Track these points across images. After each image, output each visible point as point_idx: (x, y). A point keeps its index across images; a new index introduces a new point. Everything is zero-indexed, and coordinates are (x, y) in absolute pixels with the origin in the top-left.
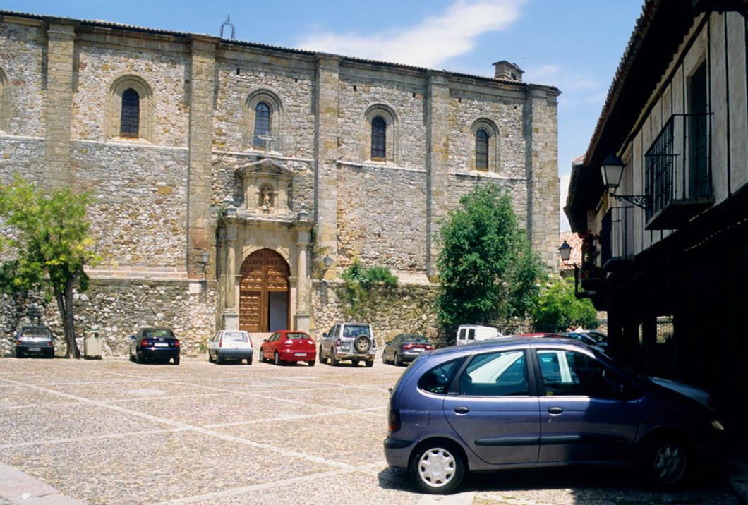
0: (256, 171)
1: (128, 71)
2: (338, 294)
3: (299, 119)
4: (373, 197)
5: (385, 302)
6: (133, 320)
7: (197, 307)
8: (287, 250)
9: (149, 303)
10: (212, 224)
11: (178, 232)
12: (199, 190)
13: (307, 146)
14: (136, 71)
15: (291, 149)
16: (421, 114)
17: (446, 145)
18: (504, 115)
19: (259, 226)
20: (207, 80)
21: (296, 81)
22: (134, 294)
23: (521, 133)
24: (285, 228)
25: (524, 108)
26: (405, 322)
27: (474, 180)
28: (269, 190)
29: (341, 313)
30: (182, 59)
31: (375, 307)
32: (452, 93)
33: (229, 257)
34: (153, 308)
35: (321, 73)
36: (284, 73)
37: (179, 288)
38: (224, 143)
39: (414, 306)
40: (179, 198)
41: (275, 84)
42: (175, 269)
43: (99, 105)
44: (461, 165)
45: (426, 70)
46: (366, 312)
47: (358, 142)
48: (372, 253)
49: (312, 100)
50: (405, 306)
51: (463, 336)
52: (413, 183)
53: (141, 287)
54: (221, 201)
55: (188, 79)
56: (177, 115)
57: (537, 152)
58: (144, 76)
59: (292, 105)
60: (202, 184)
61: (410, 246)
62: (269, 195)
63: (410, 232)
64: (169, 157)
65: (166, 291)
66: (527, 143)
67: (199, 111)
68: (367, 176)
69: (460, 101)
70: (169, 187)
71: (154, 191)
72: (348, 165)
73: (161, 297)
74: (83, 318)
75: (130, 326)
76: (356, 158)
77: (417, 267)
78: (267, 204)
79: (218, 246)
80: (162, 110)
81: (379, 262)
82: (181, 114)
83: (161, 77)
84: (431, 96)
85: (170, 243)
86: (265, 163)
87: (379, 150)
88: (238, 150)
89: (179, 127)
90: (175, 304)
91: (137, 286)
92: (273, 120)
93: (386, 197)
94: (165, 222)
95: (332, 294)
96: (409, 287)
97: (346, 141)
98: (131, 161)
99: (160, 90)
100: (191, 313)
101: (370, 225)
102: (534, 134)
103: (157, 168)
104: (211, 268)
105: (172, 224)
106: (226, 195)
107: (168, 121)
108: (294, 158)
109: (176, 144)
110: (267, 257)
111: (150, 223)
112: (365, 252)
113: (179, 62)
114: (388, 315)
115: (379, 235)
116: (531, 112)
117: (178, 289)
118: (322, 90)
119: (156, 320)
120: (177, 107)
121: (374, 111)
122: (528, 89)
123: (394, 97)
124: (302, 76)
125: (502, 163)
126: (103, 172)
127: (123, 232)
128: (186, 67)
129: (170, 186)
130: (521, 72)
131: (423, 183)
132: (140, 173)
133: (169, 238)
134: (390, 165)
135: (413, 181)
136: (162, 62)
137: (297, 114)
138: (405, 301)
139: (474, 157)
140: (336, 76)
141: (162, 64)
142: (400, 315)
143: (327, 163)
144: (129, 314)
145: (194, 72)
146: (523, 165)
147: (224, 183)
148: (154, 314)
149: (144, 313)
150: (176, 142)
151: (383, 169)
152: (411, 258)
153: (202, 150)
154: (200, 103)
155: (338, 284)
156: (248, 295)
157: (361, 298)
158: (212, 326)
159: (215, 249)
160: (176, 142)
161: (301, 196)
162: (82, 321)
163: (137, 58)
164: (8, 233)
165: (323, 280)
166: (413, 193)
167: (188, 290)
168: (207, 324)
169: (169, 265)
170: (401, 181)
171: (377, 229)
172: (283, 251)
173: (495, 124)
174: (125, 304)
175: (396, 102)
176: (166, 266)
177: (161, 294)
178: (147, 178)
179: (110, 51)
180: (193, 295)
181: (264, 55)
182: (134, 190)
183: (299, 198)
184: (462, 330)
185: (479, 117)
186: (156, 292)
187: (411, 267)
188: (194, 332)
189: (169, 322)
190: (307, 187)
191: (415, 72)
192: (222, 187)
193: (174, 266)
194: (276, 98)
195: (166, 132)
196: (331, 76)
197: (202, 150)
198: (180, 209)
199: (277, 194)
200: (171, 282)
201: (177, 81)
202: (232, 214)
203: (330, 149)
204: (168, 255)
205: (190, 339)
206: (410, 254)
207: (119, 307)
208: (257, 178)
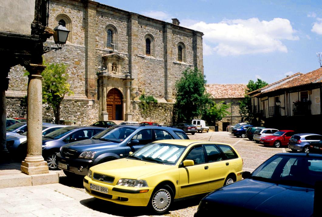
0: (111, 57)
1: (62, 12)
2: (139, 106)
3: (123, 37)
4: (148, 69)
5: (154, 109)
6: (69, 116)
7: (92, 111)
8: (122, 89)
9: (74, 109)
10: (96, 78)
11: (82, 80)
12: (91, 64)
13: (126, 48)
14: (65, 12)
15: (120, 49)
16: (162, 39)
17: (171, 51)
18: (187, 41)
19: (113, 79)
20: (93, 19)
21: (122, 22)
22: (69, 105)
23: (192, 48)
24: (122, 80)
25: (193, 39)
26: (160, 116)
27: (179, 65)
28: (115, 65)
29: (140, 113)
30: (82, 9)
31: (151, 111)
32: (174, 33)
33: (104, 91)
34: (76, 111)
35: (132, 20)
36: (118, 19)
37: (86, 103)
38: (97, 45)
39: (163, 111)
40: (83, 66)
41: (115, 23)
42: (82, 95)
43: (51, 25)
44: (174, 59)
45: (164, 22)
46: (148, 113)
47: (142, 48)
48: (148, 91)
49: (127, 31)
50: (160, 111)
51: (195, 123)
53: (71, 102)
54: (97, 68)
55: (84, 18)
56: (81, 32)
57: (198, 56)
58: (68, 15)
59: (121, 32)
60: (92, 61)
61: (159, 88)
62: (115, 67)
63: (159, 83)
64: (78, 49)
65: (81, 104)
66: (194, 52)
67: (91, 32)
68: (146, 61)
69: (174, 35)
70: (79, 62)
71: (73, 63)
72: (140, 56)
73: (79, 106)
74: (50, 114)
75: (67, 118)
76: (142, 54)
77: (162, 96)
78: (115, 71)
79: (98, 86)
80: (75, 30)
81: (150, 94)
82: (82, 32)
83: (75, 16)
84: (167, 32)
85: (80, 84)
86: (115, 54)
87: (148, 52)
88: (103, 49)
89: (82, 37)
90: (84, 109)
91: (70, 102)
92: (114, 37)
93: (152, 70)
94: (78, 76)
95: (137, 106)
96: (161, 104)
98: (65, 50)
99: (74, 21)
100: (90, 113)
101: (147, 80)
102: (197, 49)
103: (74, 54)
104: (96, 96)
105: (80, 76)
106: (99, 66)
107: (77, 34)
108: (121, 53)
109: (80, 44)
110: (115, 92)
111: (72, 76)
113: (81, 10)
114: (155, 114)
115: (150, 84)
116: (196, 41)
117: (85, 103)
118: (132, 27)
119: (77, 116)
120: (81, 29)
121: (108, 28)
122: (195, 32)
123: (153, 32)
124: (124, 21)
125: (187, 59)
126: (54, 54)
128: (83, 13)
129: (79, 61)
130: (179, 23)
131: (163, 65)
132: (68, 55)
133: (79, 82)
134: (152, 57)
136: (75, 10)
137: (122, 35)
138: (160, 109)
139: (178, 56)
140: (137, 22)
141: (75, 11)
142: (158, 114)
143: (134, 56)
144: (67, 113)
145: (89, 16)
146: (193, 60)
147: (98, 61)
148: (76, 113)
149: (73, 113)
150: (80, 43)
151: (151, 59)
152: (160, 93)
153: (92, 48)
154: (91, 29)
155: (139, 102)
156: (110, 106)
157: (146, 107)
158: (97, 118)
159: (97, 87)
160: (80, 43)
161: (124, 68)
162: (49, 115)
163: (65, 7)
164: (17, 78)
165: (134, 100)
166: (160, 69)
167: (88, 104)
168: (95, 117)
169: (79, 93)
170: (157, 64)
171: (149, 82)
172: (121, 89)
173: (184, 45)
174: (66, 109)
175: (154, 33)
176: (78, 93)
177: (79, 105)
178: (71, 58)
179: (56, 3)
180: (90, 106)
181: (111, 11)
183: (124, 68)
184: (194, 121)
185: (180, 41)
186: (77, 104)
187: (160, 96)
188: (91, 120)
189: (82, 116)
190: (126, 65)
191: (161, 22)
192: (98, 62)
193: (81, 93)
194: (115, 28)
195: (77, 39)
196: (135, 22)
197: (92, 48)
198: (83, 71)
199: (118, 67)
200: (82, 100)
201: (80, 18)
202: (105, 74)
203: (135, 50)
204: (79, 89)
205: (90, 123)
206: (160, 91)
207: (64, 110)
208: (111, 60)
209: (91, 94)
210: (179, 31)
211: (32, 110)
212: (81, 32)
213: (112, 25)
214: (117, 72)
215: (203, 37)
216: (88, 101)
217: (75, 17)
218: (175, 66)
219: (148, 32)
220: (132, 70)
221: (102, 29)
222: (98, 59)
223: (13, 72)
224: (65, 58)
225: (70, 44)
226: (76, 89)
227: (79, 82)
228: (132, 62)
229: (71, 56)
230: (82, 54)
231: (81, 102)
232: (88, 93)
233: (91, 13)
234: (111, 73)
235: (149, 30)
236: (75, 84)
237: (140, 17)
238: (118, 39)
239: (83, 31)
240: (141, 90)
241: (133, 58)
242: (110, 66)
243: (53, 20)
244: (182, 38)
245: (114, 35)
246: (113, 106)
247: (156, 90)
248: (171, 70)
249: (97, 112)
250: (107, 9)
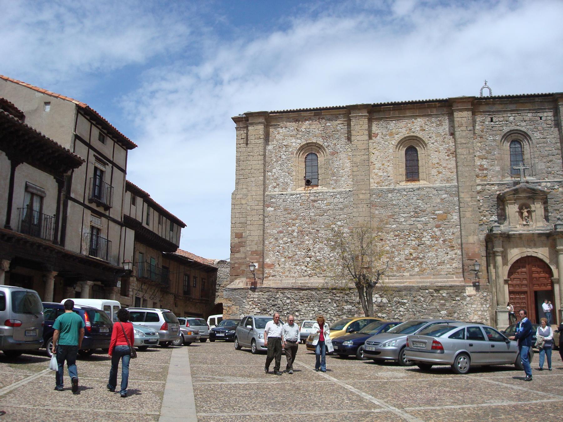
3: (547, 149)
9: (434, 303)
14: (414, 132)
28: (526, 208)
34: (438, 307)
42: (454, 276)
43: (389, 161)
56: (447, 160)
60: (470, 209)
70: (445, 214)
71: (434, 219)
73: (443, 298)
85: (449, 257)
94: (444, 241)
98: (415, 198)
99: (433, 143)
100: (469, 310)
111: (433, 242)
127: (412, 251)
158: (486, 320)
159: (485, 259)
164: (331, 257)
178: (428, 210)
180: (469, 296)
182: (419, 219)
183: (555, 212)
195: (439, 173)
200: (450, 287)
209: (473, 272)
212: (447, 160)
216: (463, 288)
217: (434, 135)
221: (493, 144)
222: (488, 202)
226: (442, 267)
230: (451, 198)
231: (449, 291)
233: (460, 119)
239: (451, 157)
243: (391, 151)
249: (486, 309)
250: (501, 104)
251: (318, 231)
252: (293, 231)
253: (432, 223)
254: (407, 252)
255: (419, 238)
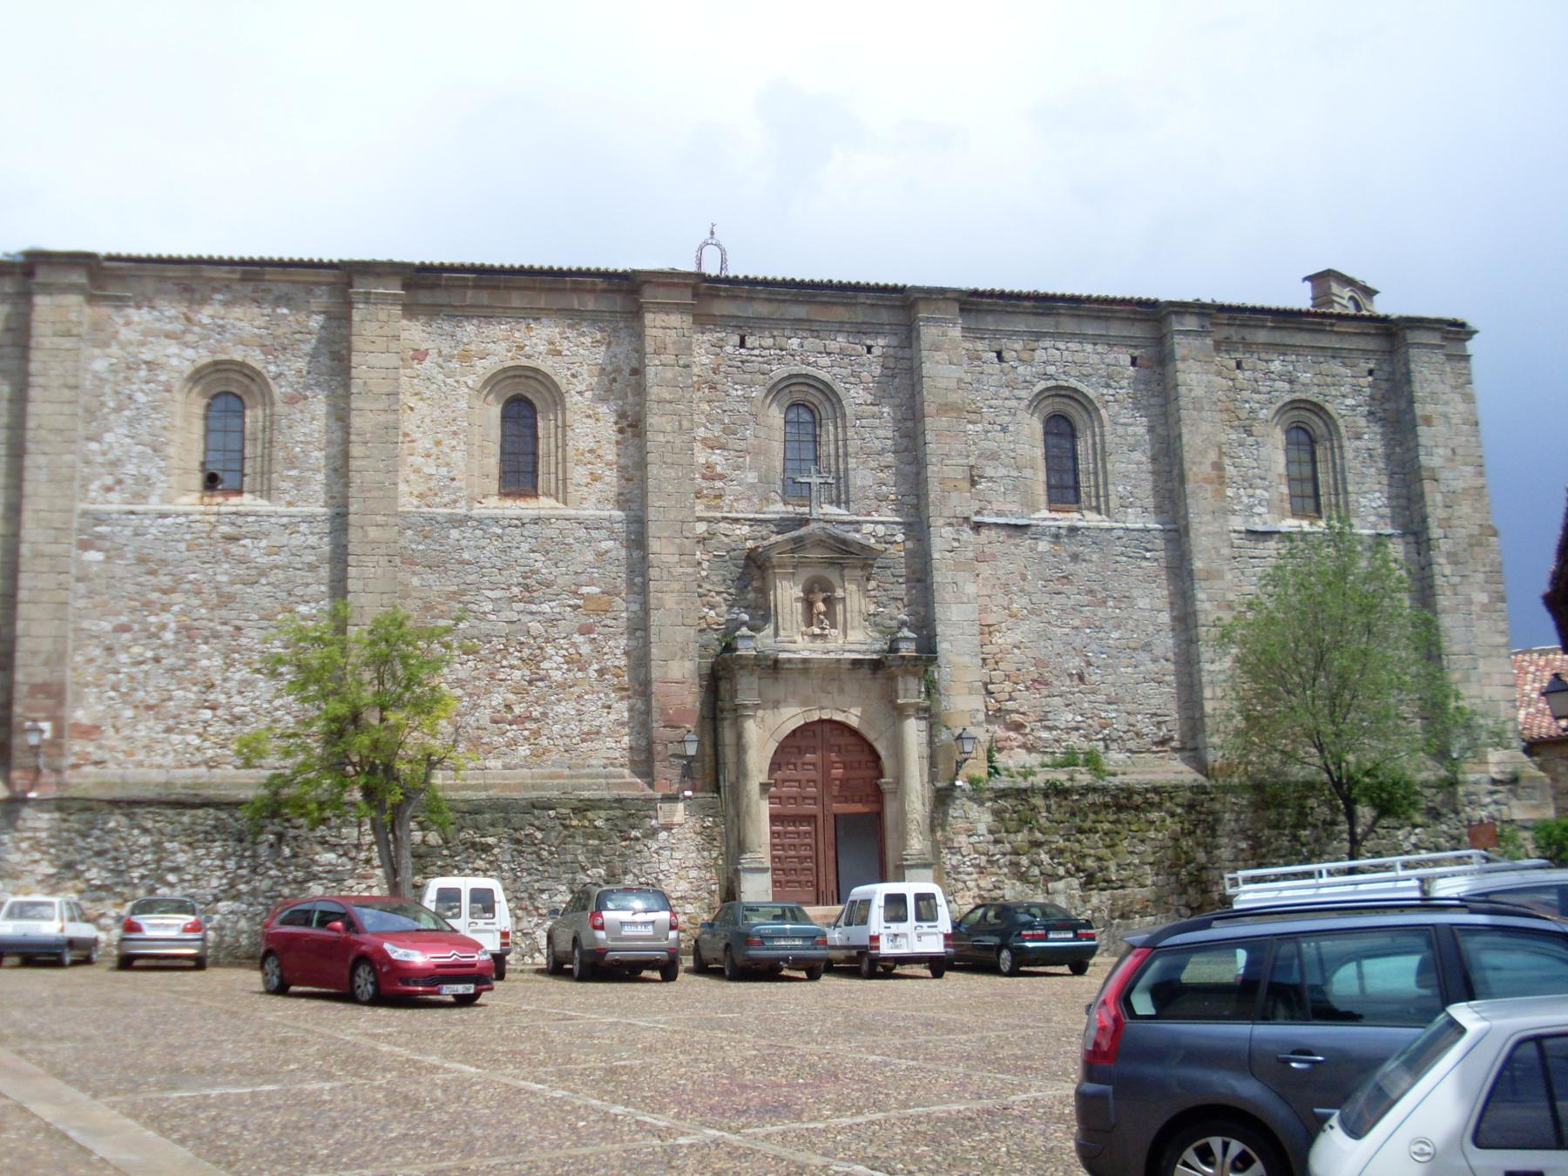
6: (537, 885)
12: (670, 601)
14: (529, 357)
22: (538, 829)
24: (866, 671)
35: (923, 330)
41: (824, 361)
43: (455, 433)
44: (1258, 510)
45: (1152, 304)
47: (1015, 473)
52: (1148, 555)
58: (546, 365)
60: (676, 586)
63: (1151, 666)
70: (606, 597)
71: (575, 607)
72: (997, 525)
73: (596, 833)
75: (531, 897)
85: (613, 717)
93: (1091, 592)
94: (601, 672)
97: (989, 472)
98: (525, 547)
100: (663, 867)
108: (876, 518)
111: (571, 675)
112: (1050, 716)
115: (1081, 678)
125: (1352, 498)
129: (608, 594)
133: (609, 707)
135: (1148, 550)
139: (1285, 490)
140: (956, 332)
143: (950, 524)
153: (672, 515)
164: (277, 709)
169: (612, 765)
171: (1075, 664)
181: (797, 302)
182: (534, 608)
185: (1287, 398)
194: (827, 390)
199: (844, 599)
203: (953, 495)
206: (1155, 714)
210: (1278, 337)
211: (1020, 779)
213: (807, 376)
214: (840, 627)
215: (1471, 346)
218: (1257, 553)
219: (1051, 377)
220: (938, 608)
223: (255, 680)
224: (527, 587)
225: (556, 512)
227: (609, 707)
228: (936, 564)
229: (561, 576)
232: (658, 758)
233: (660, 333)
234: (799, 638)
235: (498, 344)
236: (585, 717)
237: (977, 305)
238: (845, 446)
240: (1016, 717)
241: (942, 537)
242: (787, 603)
244: (1306, 377)
245: (829, 432)
246: (820, 823)
247: (1130, 707)
248: (1222, 578)
251: (238, 628)
252: (164, 627)
253: (571, 620)
254: (497, 700)
255: (533, 661)
